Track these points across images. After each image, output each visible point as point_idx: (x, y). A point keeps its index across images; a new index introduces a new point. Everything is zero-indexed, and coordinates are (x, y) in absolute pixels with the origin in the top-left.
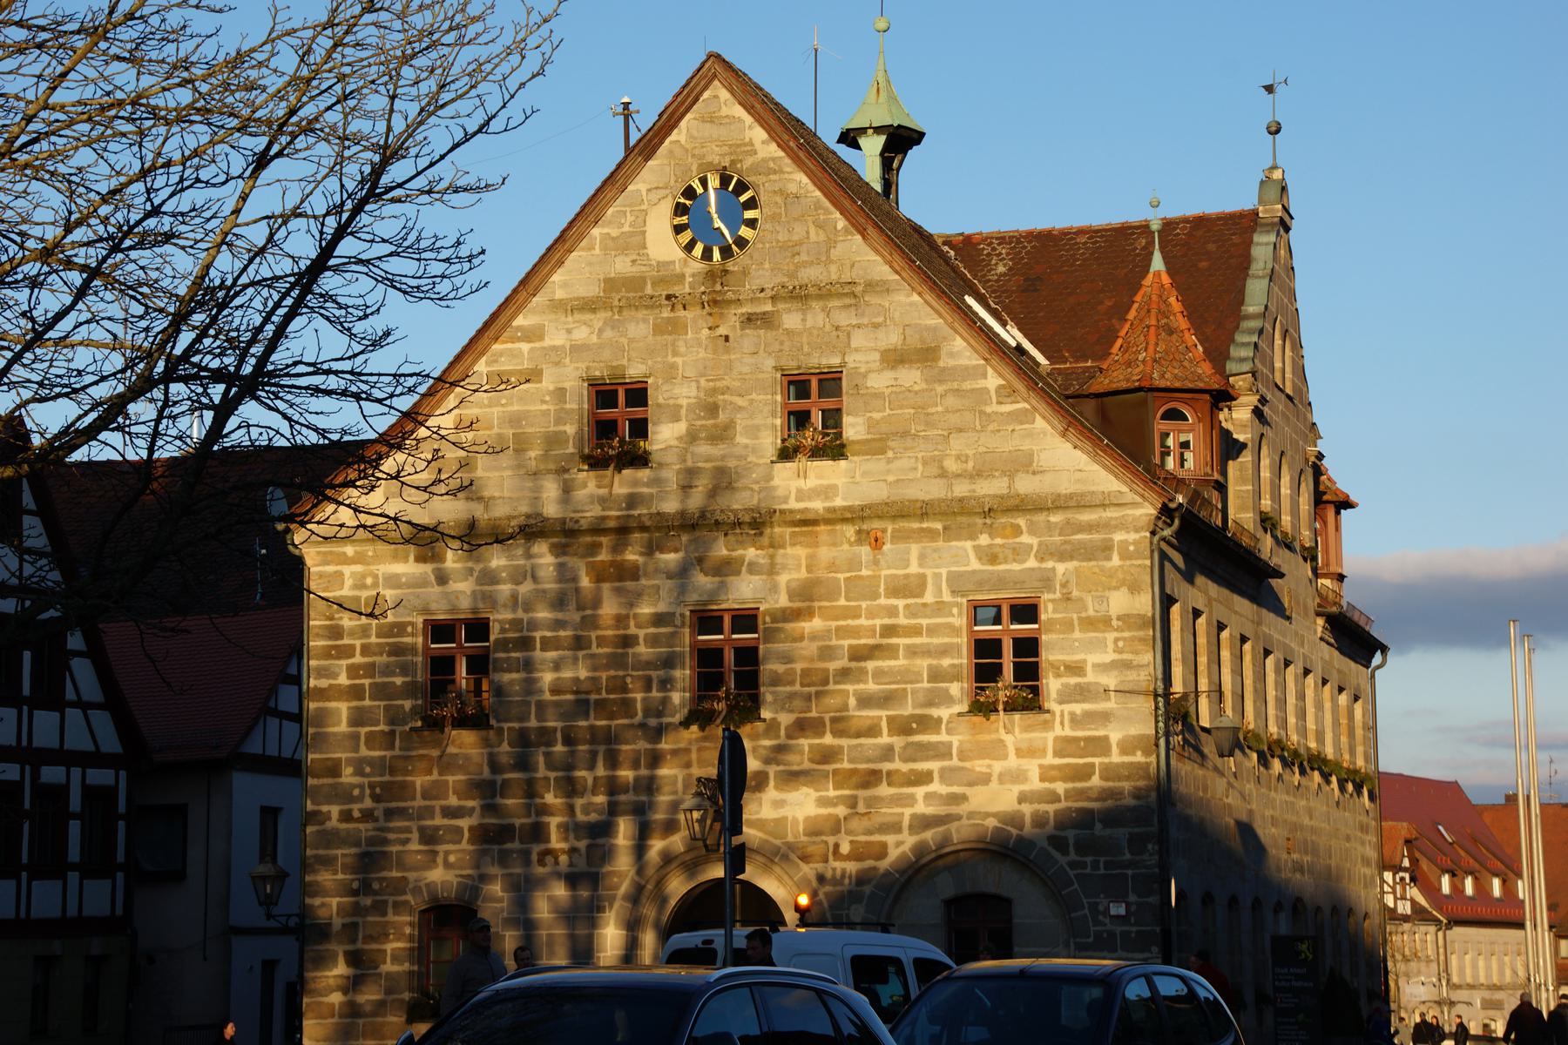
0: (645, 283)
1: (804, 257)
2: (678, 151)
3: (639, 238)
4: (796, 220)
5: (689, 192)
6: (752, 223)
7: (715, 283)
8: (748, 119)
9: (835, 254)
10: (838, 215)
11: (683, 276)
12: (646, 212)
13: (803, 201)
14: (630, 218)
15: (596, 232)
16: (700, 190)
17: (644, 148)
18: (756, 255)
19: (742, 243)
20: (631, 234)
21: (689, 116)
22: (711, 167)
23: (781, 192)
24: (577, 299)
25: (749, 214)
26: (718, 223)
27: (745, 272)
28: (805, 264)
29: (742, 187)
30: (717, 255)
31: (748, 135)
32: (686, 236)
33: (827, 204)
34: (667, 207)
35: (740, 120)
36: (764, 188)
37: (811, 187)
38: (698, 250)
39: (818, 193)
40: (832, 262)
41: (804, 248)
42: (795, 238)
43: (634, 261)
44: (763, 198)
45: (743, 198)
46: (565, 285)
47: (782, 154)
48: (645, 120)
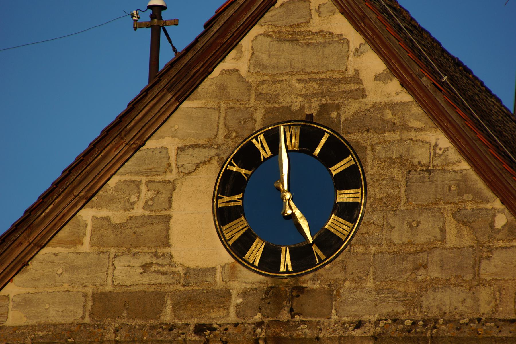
0: (163, 304)
1: (434, 272)
2: (234, 88)
3: (159, 228)
4: (425, 208)
5: (247, 155)
6: (349, 211)
7: (280, 308)
8: (355, 39)
9: (489, 269)
10: (498, 204)
11: (227, 294)
12: (172, 185)
13: (438, 177)
14: (146, 194)
15: (87, 214)
16: (265, 153)
17: (176, 79)
18: (351, 266)
19: (329, 243)
20: (146, 221)
21: (256, 30)
22: (291, 118)
23: (402, 161)
24: (45, 327)
25: (345, 196)
26: (292, 209)
27: (332, 293)
28: (435, 284)
29: (337, 149)
30: (286, 261)
31: (353, 64)
32: (237, 229)
33: (480, 184)
34: (207, 179)
35: (342, 39)
36: (376, 154)
37: (453, 155)
38: (256, 252)
39: (465, 166)
40: (483, 283)
41: (436, 256)
42: (421, 239)
43: (146, 267)
44: (371, 170)
45: (337, 169)
46: (25, 302)
47: (406, 97)
48: (183, 35)
